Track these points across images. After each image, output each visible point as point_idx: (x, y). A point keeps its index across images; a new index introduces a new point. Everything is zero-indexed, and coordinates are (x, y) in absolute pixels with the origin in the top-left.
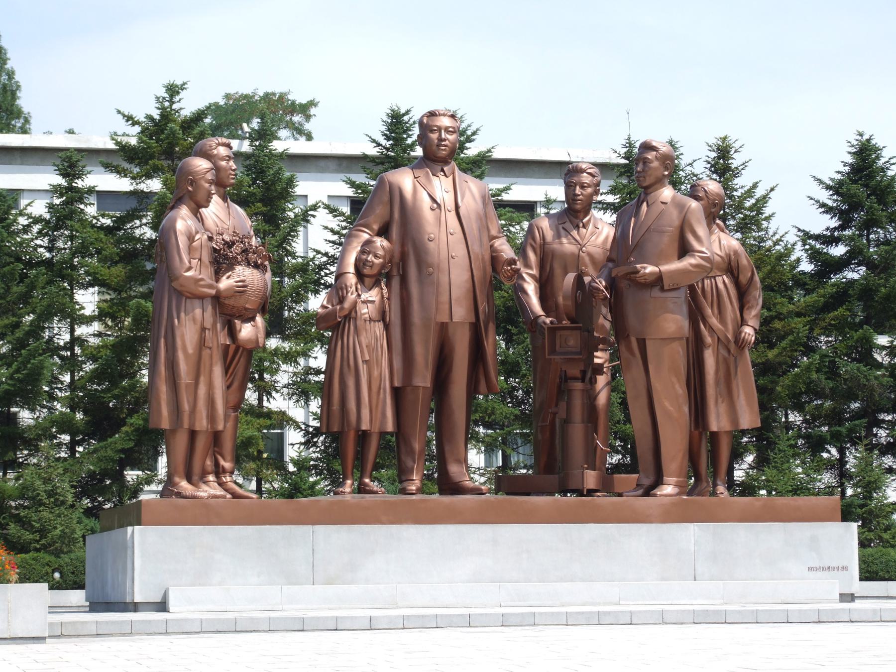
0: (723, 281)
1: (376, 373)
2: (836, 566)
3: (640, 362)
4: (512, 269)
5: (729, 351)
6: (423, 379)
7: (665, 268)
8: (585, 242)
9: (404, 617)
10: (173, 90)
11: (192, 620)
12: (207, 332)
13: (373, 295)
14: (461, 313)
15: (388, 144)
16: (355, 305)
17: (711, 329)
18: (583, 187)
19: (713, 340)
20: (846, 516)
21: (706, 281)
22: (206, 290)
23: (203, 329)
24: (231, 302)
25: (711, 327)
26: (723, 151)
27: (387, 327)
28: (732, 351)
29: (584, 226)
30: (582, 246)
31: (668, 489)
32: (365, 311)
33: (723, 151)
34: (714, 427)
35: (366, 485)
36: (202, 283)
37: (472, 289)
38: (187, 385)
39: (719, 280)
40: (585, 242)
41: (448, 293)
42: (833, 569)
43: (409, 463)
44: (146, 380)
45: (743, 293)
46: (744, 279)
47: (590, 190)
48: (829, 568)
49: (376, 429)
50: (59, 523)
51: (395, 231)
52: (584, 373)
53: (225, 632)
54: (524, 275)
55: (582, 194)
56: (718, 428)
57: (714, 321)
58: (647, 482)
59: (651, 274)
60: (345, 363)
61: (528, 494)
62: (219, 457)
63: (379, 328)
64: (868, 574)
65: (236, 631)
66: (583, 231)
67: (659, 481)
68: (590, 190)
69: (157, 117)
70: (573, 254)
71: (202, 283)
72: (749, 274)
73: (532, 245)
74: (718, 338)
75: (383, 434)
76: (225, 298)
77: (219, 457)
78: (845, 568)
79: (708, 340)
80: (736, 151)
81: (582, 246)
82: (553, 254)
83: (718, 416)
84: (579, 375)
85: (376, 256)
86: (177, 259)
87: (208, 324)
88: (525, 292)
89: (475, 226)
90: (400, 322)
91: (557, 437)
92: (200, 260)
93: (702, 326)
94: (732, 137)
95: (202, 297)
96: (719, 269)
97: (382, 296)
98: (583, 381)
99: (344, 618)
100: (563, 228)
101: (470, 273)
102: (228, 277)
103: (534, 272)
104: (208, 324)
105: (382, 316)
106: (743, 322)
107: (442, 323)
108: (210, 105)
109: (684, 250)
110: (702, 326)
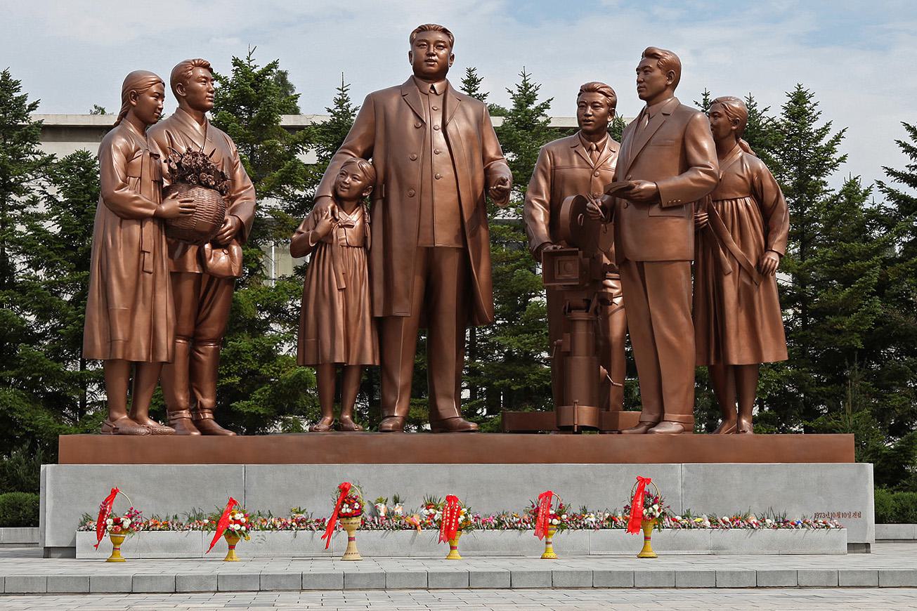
0: (745, 203)
1: (352, 302)
3: (641, 285)
4: (497, 188)
5: (751, 279)
6: (407, 309)
7: (664, 184)
8: (598, 165)
12: (146, 254)
13: (355, 218)
14: (444, 237)
16: (330, 229)
17: (731, 255)
18: (594, 107)
19: (733, 266)
21: (726, 203)
22: (142, 210)
23: (142, 252)
24: (179, 224)
25: (731, 253)
26: (799, 98)
27: (369, 253)
28: (755, 279)
29: (597, 149)
30: (594, 170)
31: (672, 427)
32: (346, 236)
33: (799, 98)
34: (735, 361)
35: (345, 421)
36: (137, 202)
37: (459, 211)
38: (123, 312)
39: (741, 203)
40: (598, 165)
41: (430, 217)
43: (392, 398)
45: (767, 213)
46: (770, 197)
47: (602, 110)
49: (353, 362)
50: (711, 413)
51: (379, 152)
52: (588, 302)
54: (534, 202)
55: (593, 115)
56: (739, 361)
57: (735, 247)
58: (649, 418)
59: (647, 190)
60: (320, 293)
61: (536, 432)
62: (198, 393)
63: (358, 255)
66: (596, 154)
67: (659, 420)
68: (602, 110)
70: (585, 179)
71: (137, 202)
72: (775, 196)
73: (542, 171)
74: (740, 265)
75: (363, 367)
77: (198, 393)
81: (594, 170)
82: (563, 179)
83: (739, 348)
84: (583, 304)
85: (354, 178)
87: (148, 245)
88: (533, 219)
89: (464, 147)
90: (378, 245)
92: (140, 178)
95: (141, 219)
96: (741, 192)
97: (364, 221)
98: (587, 310)
100: (576, 151)
101: (456, 195)
102: (174, 197)
103: (545, 198)
104: (148, 245)
105: (364, 243)
106: (767, 248)
109: (686, 164)
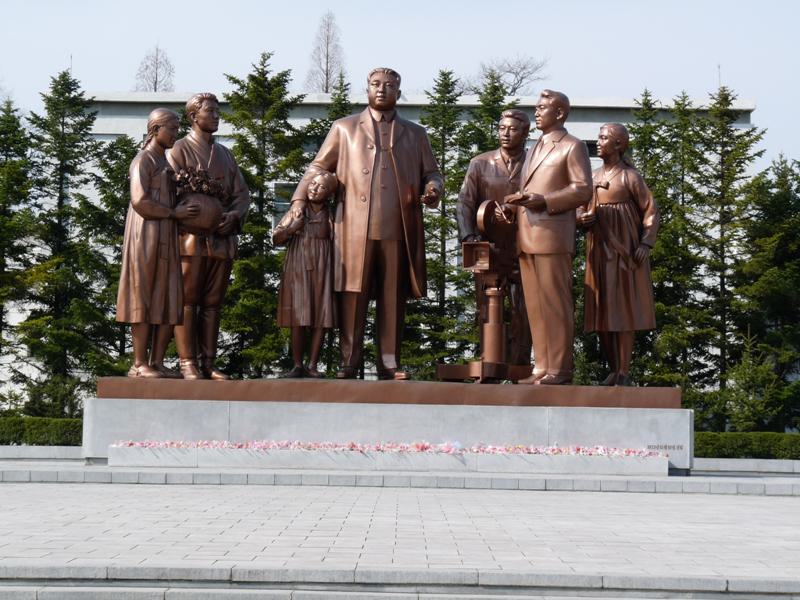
2: (672, 444)
9: (194, 475)
10: (265, 57)
11: (21, 472)
15: (437, 95)
20: (685, 404)
42: (670, 447)
44: (185, 308)
48: (666, 447)
53: (46, 482)
64: (701, 450)
65: (57, 482)
69: (269, 77)
76: (186, 218)
78: (681, 447)
79: (610, 256)
80: (733, 99)
86: (374, 220)
91: (326, 319)
93: (606, 247)
94: (730, 89)
99: (145, 475)
107: (376, 241)
108: (399, 76)
110: (606, 247)
